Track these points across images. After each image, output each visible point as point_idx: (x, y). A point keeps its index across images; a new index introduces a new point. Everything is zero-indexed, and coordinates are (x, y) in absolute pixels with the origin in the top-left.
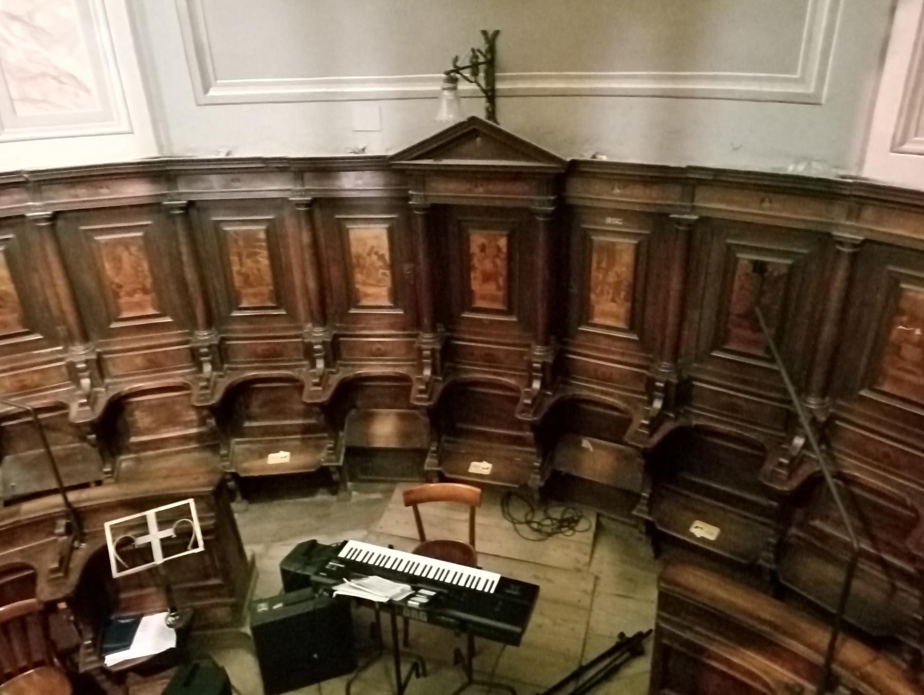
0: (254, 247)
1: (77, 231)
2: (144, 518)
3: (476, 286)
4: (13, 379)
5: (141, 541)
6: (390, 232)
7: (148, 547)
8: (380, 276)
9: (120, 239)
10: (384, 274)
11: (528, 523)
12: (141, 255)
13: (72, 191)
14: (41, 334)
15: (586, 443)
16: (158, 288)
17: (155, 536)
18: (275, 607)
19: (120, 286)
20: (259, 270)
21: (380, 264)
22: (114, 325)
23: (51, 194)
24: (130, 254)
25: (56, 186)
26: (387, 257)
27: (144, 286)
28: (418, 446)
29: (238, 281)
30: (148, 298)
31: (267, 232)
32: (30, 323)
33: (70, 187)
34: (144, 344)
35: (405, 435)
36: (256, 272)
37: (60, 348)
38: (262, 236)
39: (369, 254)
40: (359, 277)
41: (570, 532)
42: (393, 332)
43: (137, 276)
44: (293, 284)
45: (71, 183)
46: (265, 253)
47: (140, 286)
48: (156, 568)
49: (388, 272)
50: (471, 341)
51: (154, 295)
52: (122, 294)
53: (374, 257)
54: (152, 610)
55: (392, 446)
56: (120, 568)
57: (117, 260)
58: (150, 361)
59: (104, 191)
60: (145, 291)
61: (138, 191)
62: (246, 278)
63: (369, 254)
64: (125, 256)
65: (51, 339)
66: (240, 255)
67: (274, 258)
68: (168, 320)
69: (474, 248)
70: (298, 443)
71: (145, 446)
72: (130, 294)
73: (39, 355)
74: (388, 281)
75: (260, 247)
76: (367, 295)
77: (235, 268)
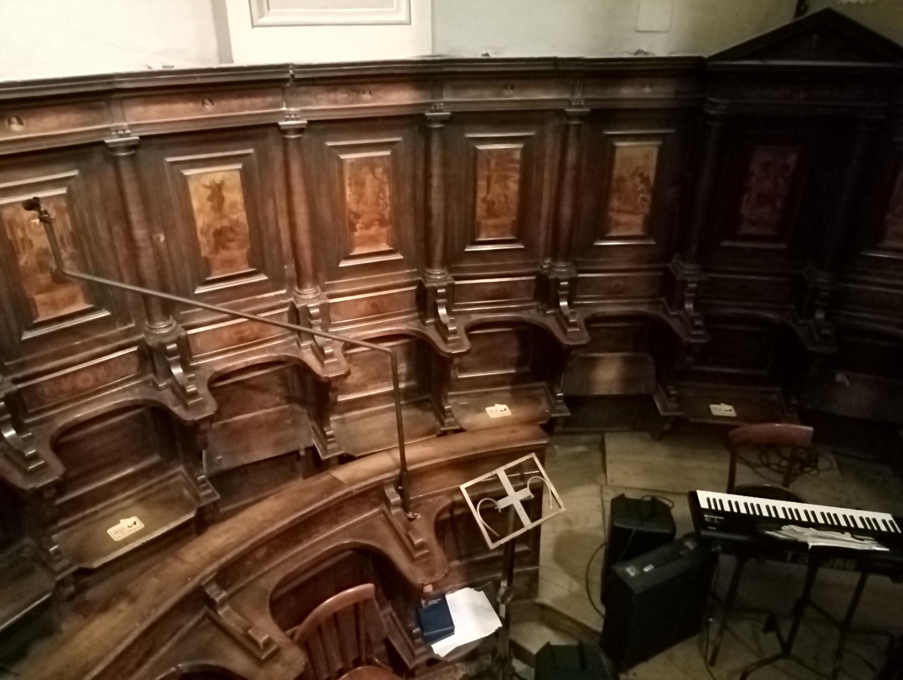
0: (507, 170)
1: (322, 146)
2: (496, 475)
3: (745, 211)
4: (233, 331)
5: (502, 504)
6: (662, 151)
7: (509, 509)
8: (639, 201)
9: (366, 158)
10: (643, 199)
11: (768, 465)
12: (385, 178)
13: (332, 96)
14: (266, 274)
15: (840, 377)
16: (395, 221)
17: (514, 498)
18: (646, 570)
19: (358, 216)
20: (506, 197)
21: (641, 187)
22: (343, 264)
23: (307, 98)
24: (375, 177)
25: (317, 88)
26: (652, 180)
27: (382, 216)
28: (643, 391)
29: (481, 210)
30: (384, 230)
31: (524, 151)
32: (258, 263)
33: (329, 91)
34: (371, 286)
35: (627, 380)
36: (502, 199)
37: (284, 291)
38: (518, 156)
39: (632, 176)
40: (615, 203)
41: (815, 472)
42: (646, 266)
43: (377, 204)
44: (539, 214)
45: (334, 84)
46: (516, 176)
47: (378, 217)
48: (528, 531)
49: (648, 197)
50: (725, 272)
51: (389, 227)
52: (358, 226)
53: (638, 180)
54: (450, 586)
55: (614, 392)
56: (494, 540)
57: (360, 184)
58: (374, 306)
59: (366, 96)
60: (382, 222)
61: (400, 98)
62: (490, 205)
63: (632, 176)
64: (369, 179)
65: (276, 282)
66: (489, 180)
67: (525, 183)
68: (262, 278)
69: (755, 167)
70: (508, 395)
71: (352, 405)
72: (367, 226)
73: (263, 300)
74: (646, 209)
75: (513, 170)
76: (618, 224)
77: (481, 194)
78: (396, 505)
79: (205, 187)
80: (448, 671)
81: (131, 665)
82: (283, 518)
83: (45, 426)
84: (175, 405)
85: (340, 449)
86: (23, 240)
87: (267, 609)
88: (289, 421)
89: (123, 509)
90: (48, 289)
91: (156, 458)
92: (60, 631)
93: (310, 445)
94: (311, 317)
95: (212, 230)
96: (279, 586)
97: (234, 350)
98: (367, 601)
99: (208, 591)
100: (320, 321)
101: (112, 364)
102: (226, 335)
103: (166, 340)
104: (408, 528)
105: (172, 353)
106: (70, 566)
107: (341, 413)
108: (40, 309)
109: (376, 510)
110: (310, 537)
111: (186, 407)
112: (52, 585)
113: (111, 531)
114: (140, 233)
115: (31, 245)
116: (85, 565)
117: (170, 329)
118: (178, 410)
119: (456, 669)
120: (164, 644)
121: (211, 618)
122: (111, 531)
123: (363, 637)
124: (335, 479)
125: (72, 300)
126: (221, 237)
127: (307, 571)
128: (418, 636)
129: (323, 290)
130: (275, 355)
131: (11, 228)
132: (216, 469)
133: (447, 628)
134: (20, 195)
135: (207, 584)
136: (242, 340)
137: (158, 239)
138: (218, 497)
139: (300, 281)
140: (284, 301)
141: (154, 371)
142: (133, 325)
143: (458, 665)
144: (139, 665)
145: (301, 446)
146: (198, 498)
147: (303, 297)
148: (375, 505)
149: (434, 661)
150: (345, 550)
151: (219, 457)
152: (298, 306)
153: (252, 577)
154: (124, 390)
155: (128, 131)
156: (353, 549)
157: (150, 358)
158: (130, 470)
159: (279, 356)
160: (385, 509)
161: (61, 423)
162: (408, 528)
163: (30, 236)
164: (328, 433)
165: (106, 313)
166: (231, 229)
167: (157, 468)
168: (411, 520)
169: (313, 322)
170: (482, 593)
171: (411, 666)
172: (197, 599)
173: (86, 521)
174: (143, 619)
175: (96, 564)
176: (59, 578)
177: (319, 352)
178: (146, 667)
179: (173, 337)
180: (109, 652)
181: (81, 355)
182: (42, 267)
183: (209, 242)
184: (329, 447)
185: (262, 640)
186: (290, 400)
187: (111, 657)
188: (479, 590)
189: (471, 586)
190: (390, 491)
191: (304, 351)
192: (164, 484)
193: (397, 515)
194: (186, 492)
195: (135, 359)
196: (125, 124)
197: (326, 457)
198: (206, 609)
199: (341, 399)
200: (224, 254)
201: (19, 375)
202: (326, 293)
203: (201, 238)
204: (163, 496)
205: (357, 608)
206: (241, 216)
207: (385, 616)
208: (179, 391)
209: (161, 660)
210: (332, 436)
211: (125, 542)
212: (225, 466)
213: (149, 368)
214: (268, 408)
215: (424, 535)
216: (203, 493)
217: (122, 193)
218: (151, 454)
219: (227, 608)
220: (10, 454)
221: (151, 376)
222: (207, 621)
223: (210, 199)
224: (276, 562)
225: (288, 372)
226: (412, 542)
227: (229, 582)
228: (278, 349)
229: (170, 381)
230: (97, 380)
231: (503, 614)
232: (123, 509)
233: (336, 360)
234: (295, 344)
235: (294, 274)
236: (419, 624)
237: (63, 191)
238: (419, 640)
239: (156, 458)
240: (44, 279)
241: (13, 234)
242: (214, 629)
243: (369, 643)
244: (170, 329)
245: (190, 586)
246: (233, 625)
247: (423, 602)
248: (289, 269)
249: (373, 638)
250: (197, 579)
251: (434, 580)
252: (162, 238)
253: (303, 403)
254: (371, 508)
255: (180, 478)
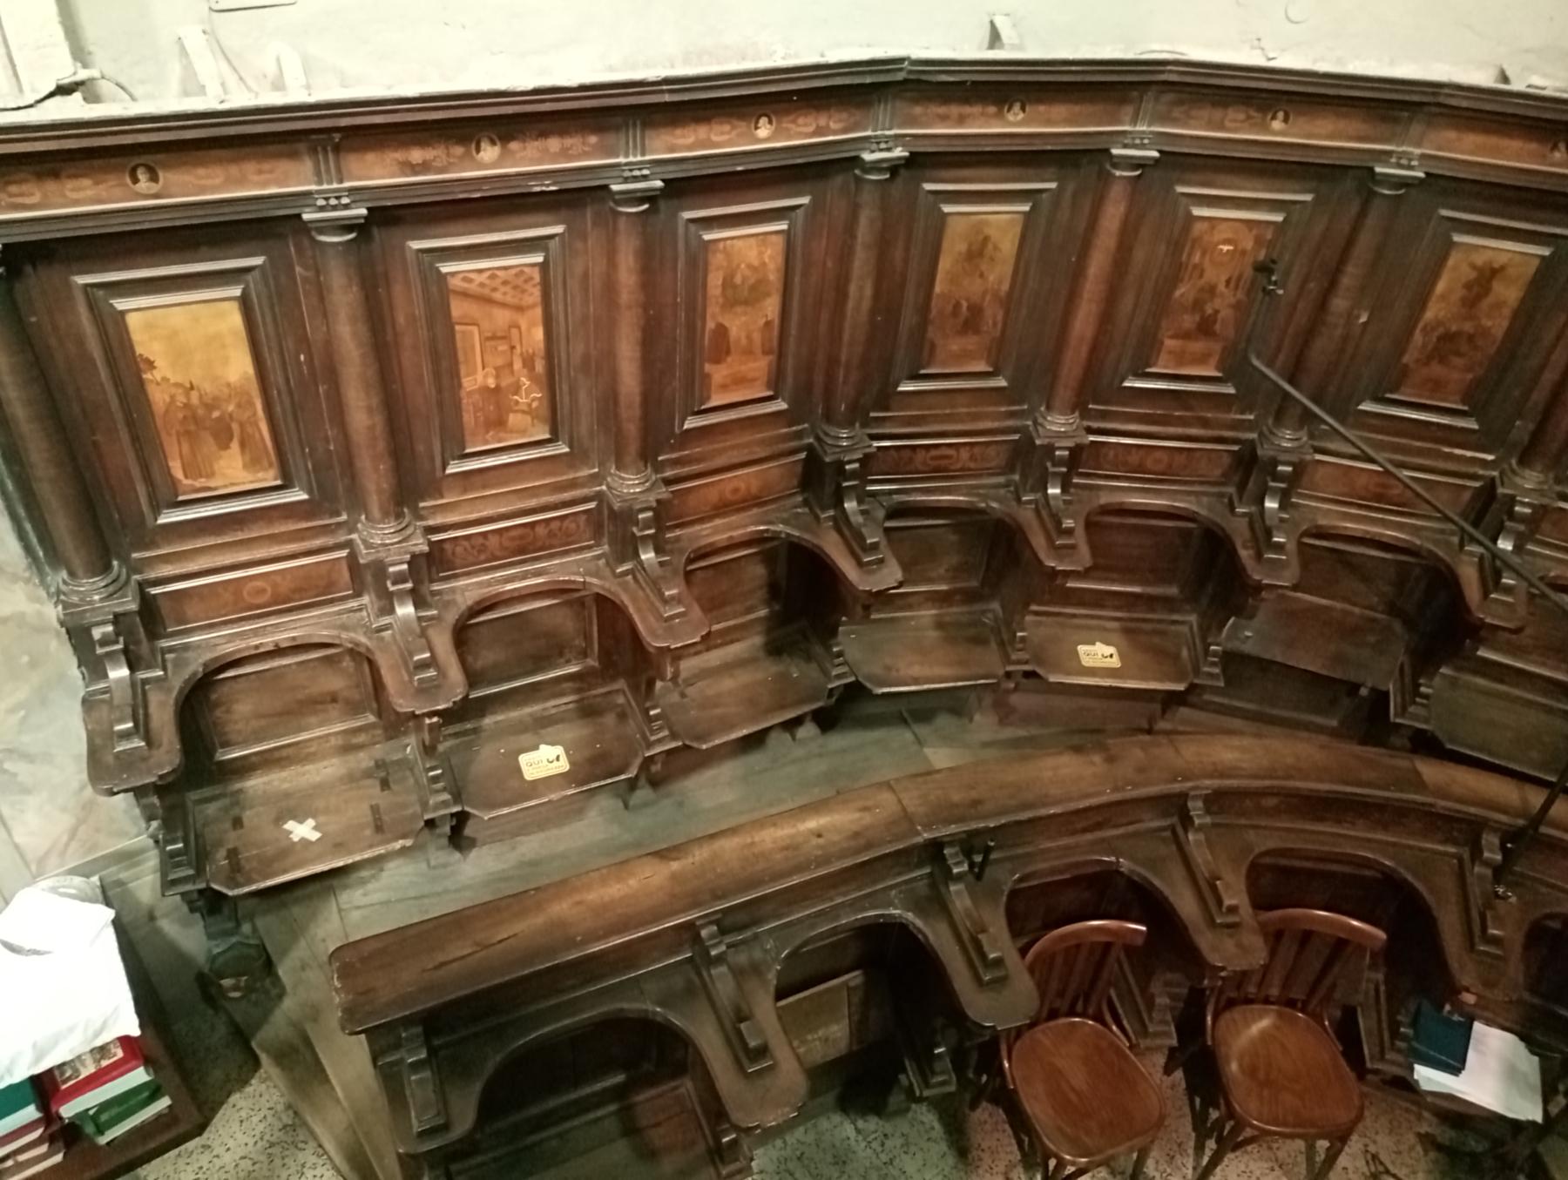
37: (1490, 457)
78: (1487, 863)
79: (1473, 267)
80: (1407, 1110)
81: (1079, 826)
82: (1320, 780)
83: (1086, 493)
84: (1245, 547)
85: (1426, 721)
86: (1195, 266)
87: (1244, 871)
88: (1372, 639)
89: (1105, 629)
90: (1186, 336)
91: (1173, 591)
92: (971, 720)
93: (1383, 688)
94: (1512, 516)
95: (1441, 330)
96: (1267, 853)
97: (1360, 506)
98: (1361, 948)
99: (1190, 804)
100: (1522, 528)
101: (1198, 454)
102: (1362, 481)
103: (1283, 457)
104: (1488, 905)
105: (1278, 477)
106: (1026, 662)
107: (1459, 669)
108: (1163, 357)
109: (1452, 849)
110: (1339, 822)
111: (1259, 556)
112: (1001, 672)
113: (1082, 649)
114: (1339, 303)
115: (1201, 276)
116: (1040, 671)
117: (1296, 444)
118: (1245, 554)
119: (1419, 1117)
120: (1116, 826)
121: (1174, 832)
122: (1082, 649)
123: (1327, 982)
124: (1418, 774)
125: (1202, 360)
126: (1446, 344)
127: (1307, 859)
128: (1405, 1038)
129: (1558, 481)
130: (1418, 542)
131: (1193, 247)
132: (1235, 645)
133: (1456, 1066)
134: (1225, 208)
135: (1196, 797)
136: (1379, 498)
137: (1358, 317)
138: (1222, 684)
139: (1526, 457)
140: (1481, 472)
141: (1242, 487)
142: (1252, 417)
143: (1426, 1114)
144: (1085, 830)
145: (1368, 682)
146: (1197, 671)
147: (1518, 480)
148: (1455, 843)
149: (1407, 1086)
150: (1370, 868)
151: (1248, 634)
152: (1501, 490)
153: (1243, 821)
154: (1189, 493)
155: (1414, 163)
156: (1383, 873)
157: (1249, 468)
158: (1136, 589)
159: (1420, 547)
160: (1466, 856)
161: (1105, 499)
162: (1488, 905)
163: (1207, 264)
164: (1423, 689)
165: (1232, 391)
166: (1471, 338)
167: (1168, 603)
168: (1497, 895)
169: (1508, 524)
170: (1536, 1059)
171: (1369, 1065)
172: (1176, 806)
173: (1060, 619)
174: (1116, 789)
175: (1053, 679)
176: (1010, 668)
177: (1492, 569)
178: (1089, 837)
179: (1294, 458)
180: (1070, 800)
181: (1171, 430)
182: (1197, 305)
183: (1424, 346)
184: (1412, 709)
185: (1228, 902)
186: (1392, 609)
187: (1073, 806)
188: (1533, 1052)
189: (1522, 1037)
190: (1490, 840)
191: (1465, 558)
192: (1159, 626)
193: (1481, 877)
194: (1185, 653)
195: (1226, 460)
196: (1418, 151)
197: (1399, 721)
198: (1175, 820)
199: (1482, 653)
200: (1436, 369)
201: (1095, 425)
202: (1558, 488)
203: (1418, 337)
204: (1156, 640)
205: (1341, 946)
206: (1498, 325)
207: (1368, 980)
208: (1261, 533)
209: (1103, 840)
210: (1426, 697)
211: (1092, 672)
212: (1248, 648)
213: (1236, 478)
214: (1355, 604)
215: (1506, 929)
216: (1206, 669)
217: (1350, 242)
218: (1170, 583)
219: (1201, 837)
220: (1044, 513)
221: (1231, 490)
222: (1168, 834)
223: (1468, 286)
224: (1279, 825)
225: (1417, 571)
226: (1484, 928)
227: (1215, 808)
228: (1425, 533)
229: (1253, 509)
230: (1170, 466)
231: (1554, 1110)
232: (1105, 629)
233: (1510, 599)
234: (1455, 540)
235: (1526, 438)
236: (1414, 1024)
237: (1279, 218)
238: (1401, 1044)
239: (1173, 591)
240: (1189, 321)
241: (1190, 255)
242: (1174, 848)
243: (1328, 998)
244: (1296, 444)
245: (1177, 787)
246: (1200, 860)
247: (1448, 1007)
248: (1522, 429)
249: (1337, 995)
250: (1189, 784)
251: (1488, 994)
252: (1363, 319)
253: (1409, 623)
254: (1445, 842)
255: (1185, 629)
